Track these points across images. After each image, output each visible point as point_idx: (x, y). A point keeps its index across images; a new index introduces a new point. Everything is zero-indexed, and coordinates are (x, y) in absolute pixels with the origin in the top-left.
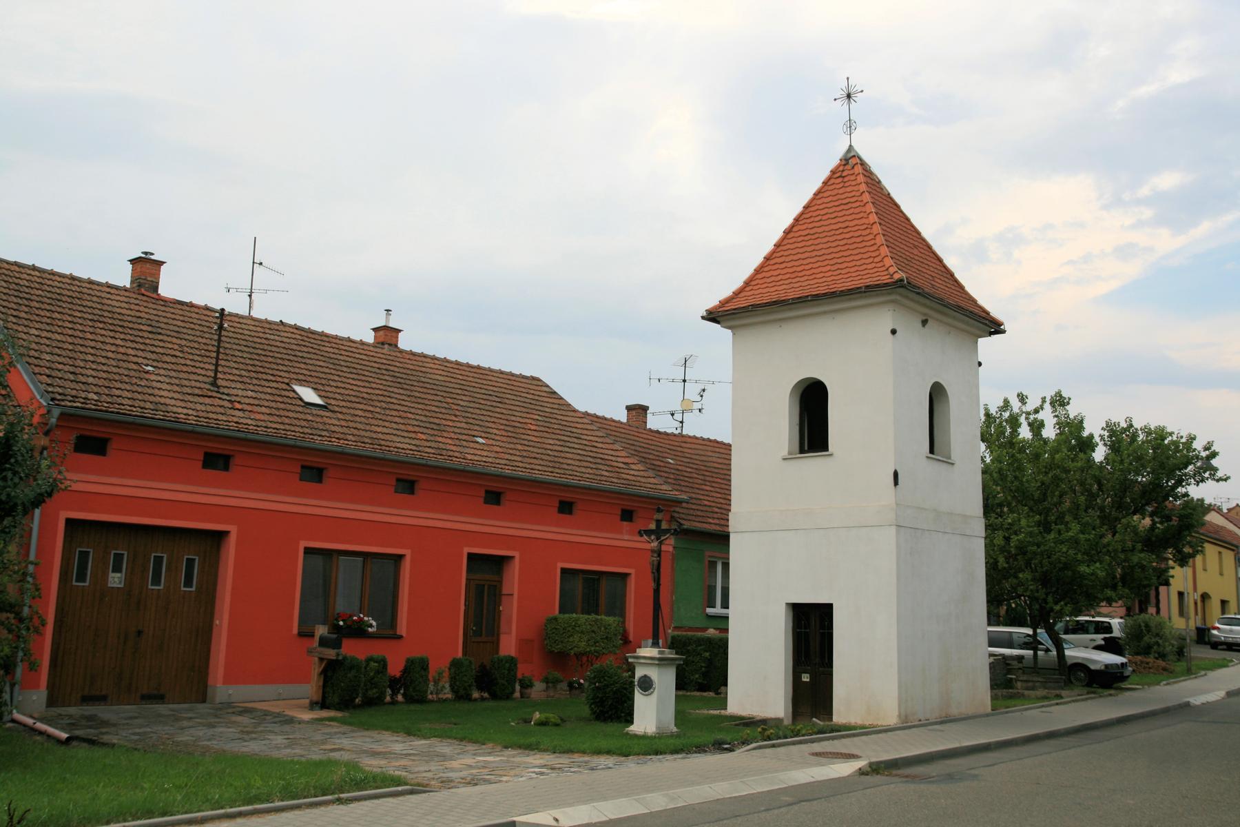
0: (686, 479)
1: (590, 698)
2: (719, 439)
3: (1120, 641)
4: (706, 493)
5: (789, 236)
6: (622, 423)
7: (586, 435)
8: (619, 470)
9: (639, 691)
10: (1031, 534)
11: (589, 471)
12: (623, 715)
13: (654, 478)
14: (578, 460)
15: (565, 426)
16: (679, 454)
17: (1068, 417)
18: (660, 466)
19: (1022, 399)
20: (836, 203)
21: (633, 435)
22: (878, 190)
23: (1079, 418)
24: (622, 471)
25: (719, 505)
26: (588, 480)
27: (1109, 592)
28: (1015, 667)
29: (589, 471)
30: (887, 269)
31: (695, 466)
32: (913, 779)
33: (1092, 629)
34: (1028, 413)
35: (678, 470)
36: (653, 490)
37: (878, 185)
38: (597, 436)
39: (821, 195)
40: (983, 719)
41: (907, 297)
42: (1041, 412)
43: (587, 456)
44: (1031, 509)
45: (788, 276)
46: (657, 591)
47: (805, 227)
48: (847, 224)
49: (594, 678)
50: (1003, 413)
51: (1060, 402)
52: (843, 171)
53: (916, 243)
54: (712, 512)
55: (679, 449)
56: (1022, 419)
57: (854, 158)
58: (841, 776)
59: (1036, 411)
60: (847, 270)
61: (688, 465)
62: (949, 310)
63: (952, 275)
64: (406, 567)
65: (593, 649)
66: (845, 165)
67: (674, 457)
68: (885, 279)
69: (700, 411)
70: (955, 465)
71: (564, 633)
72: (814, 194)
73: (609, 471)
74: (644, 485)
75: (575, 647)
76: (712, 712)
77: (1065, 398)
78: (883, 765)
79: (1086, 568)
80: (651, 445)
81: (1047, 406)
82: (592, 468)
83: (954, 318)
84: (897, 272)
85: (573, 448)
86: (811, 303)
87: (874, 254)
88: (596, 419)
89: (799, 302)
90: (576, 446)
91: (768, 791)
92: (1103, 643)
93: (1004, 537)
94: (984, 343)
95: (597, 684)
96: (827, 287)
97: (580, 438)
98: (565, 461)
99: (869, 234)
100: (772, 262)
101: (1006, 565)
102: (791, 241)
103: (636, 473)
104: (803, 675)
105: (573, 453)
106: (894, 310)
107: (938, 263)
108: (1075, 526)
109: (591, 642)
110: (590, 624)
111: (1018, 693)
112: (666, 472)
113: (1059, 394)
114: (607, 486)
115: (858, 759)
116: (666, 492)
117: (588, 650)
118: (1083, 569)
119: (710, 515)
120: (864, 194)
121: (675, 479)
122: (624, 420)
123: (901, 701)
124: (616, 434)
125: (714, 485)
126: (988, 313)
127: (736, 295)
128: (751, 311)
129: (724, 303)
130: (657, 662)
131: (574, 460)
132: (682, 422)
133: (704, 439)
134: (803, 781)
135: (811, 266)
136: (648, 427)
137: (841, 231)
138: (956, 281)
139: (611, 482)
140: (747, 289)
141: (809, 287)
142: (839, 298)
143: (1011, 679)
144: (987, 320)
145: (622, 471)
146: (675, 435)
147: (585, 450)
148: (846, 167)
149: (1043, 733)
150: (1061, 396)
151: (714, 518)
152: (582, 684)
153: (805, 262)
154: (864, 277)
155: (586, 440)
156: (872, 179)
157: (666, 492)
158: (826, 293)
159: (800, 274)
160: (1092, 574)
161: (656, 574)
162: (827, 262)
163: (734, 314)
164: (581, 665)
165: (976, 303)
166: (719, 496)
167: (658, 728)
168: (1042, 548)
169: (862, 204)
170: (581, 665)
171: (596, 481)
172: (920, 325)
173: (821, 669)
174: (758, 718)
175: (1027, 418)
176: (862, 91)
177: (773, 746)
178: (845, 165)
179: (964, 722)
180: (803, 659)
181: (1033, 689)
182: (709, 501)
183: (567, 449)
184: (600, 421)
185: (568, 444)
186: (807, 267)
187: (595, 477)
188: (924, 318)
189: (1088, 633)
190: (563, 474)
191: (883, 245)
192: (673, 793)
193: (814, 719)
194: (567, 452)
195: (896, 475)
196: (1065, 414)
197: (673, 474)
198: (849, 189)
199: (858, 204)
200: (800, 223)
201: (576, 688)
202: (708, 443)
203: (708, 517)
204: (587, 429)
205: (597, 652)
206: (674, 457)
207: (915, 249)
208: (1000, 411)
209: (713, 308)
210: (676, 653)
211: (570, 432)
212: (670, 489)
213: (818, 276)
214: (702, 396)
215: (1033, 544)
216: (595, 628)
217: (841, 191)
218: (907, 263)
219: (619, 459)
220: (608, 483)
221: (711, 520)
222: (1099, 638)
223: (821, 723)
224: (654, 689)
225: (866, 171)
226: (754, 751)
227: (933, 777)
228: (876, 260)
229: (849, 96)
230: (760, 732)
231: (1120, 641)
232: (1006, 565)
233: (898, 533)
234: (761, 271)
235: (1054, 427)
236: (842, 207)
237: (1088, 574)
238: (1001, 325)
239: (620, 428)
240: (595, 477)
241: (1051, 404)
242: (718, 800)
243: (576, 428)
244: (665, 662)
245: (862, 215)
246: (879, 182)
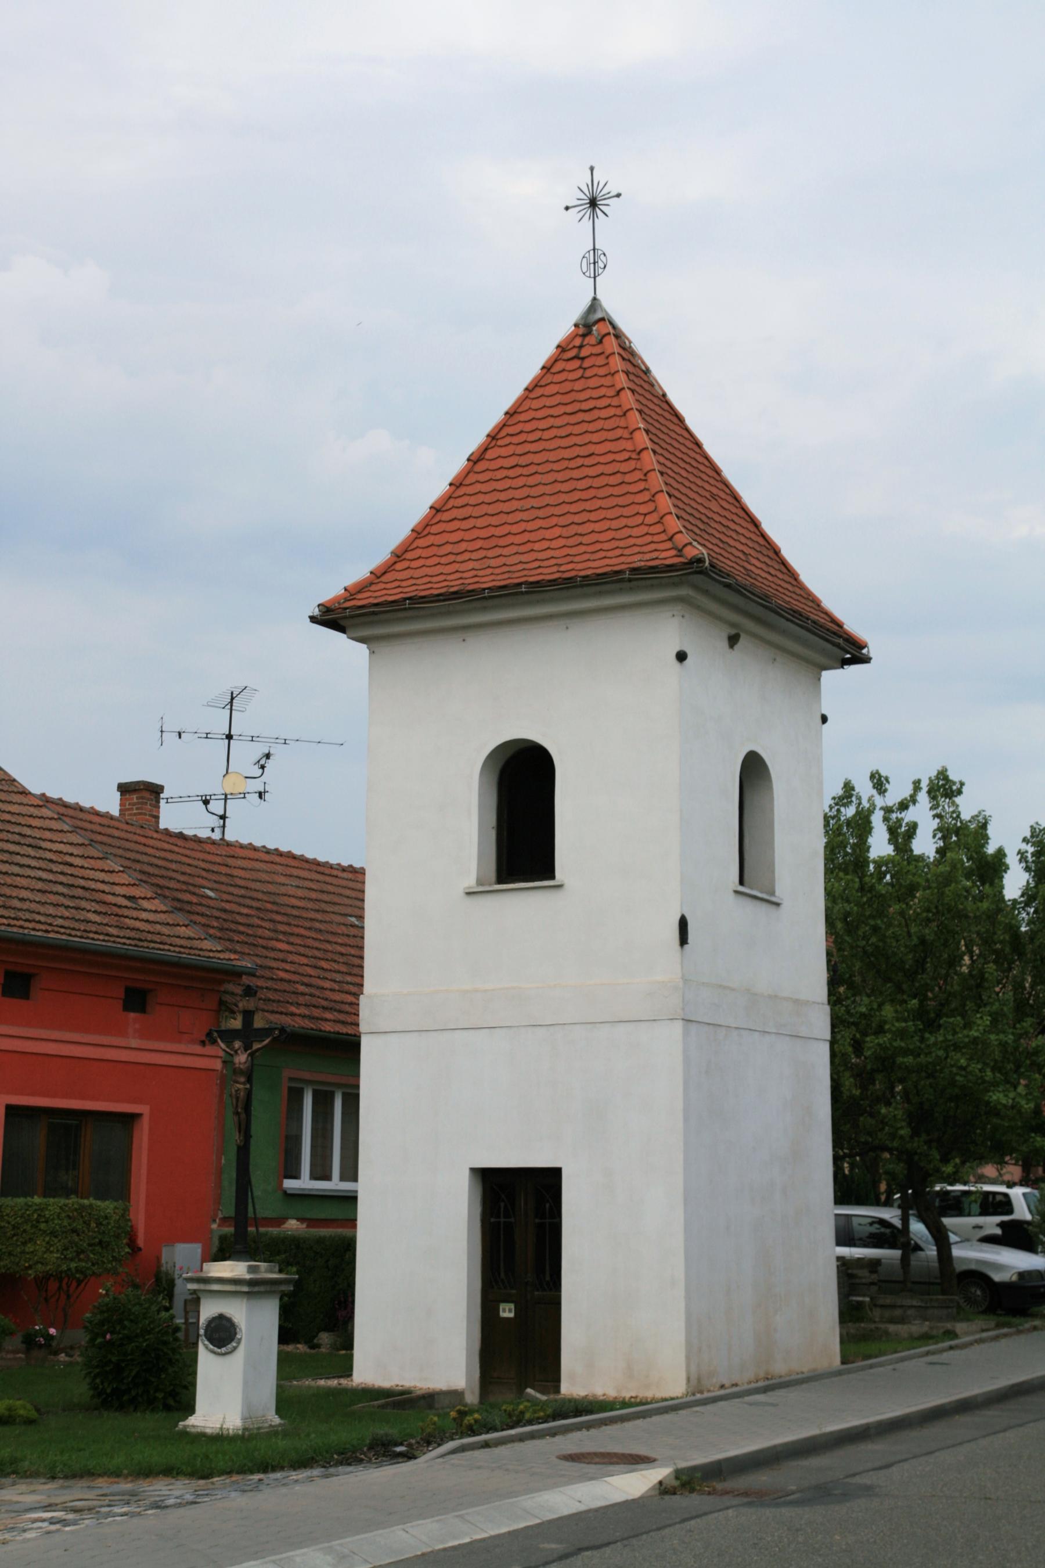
0: (241, 928)
1: (95, 1363)
2: (297, 852)
3: (1030, 1228)
4: (281, 955)
5: (481, 466)
6: (112, 818)
7: (51, 841)
8: (120, 912)
9: (207, 1348)
10: (902, 1034)
11: (62, 911)
12: (160, 1395)
13: (186, 926)
14: (38, 891)
15: (9, 822)
16: (223, 879)
17: (958, 816)
18: (189, 903)
19: (879, 782)
20: (569, 409)
21: (136, 842)
22: (646, 386)
23: (980, 818)
24: (126, 912)
25: (306, 980)
26: (62, 930)
27: (1039, 1139)
28: (864, 1281)
29: (62, 911)
30: (671, 539)
31: (254, 904)
32: (757, 1498)
33: (976, 1208)
34: (888, 810)
35: (225, 911)
36: (187, 951)
37: (645, 378)
38: (71, 844)
39: (538, 392)
40: (834, 1379)
41: (706, 592)
42: (911, 808)
43: (56, 882)
44: (899, 989)
45: (479, 544)
46: (243, 1152)
47: (510, 450)
48: (591, 449)
49: (102, 1323)
50: (842, 809)
51: (945, 789)
52: (581, 347)
53: (715, 491)
54: (294, 993)
55: (224, 870)
56: (877, 819)
57: (601, 323)
58: (630, 1498)
59: (903, 806)
60: (595, 537)
61: (242, 900)
62: (777, 617)
63: (777, 552)
64: (143, 1136)
65: (73, 1265)
66: (584, 336)
67: (215, 886)
68: (668, 557)
69: (260, 797)
70: (782, 906)
71: (14, 1235)
72: (527, 389)
73: (101, 913)
74: (168, 940)
75: (37, 1262)
76: (322, 1382)
77: (954, 783)
78: (698, 1475)
79: (1001, 1095)
80: (172, 861)
81: (923, 797)
82: (67, 907)
83: (784, 632)
84: (690, 544)
85: (29, 866)
86: (526, 597)
87: (643, 509)
88: (63, 810)
89: (501, 596)
90: (34, 863)
91: (509, 1532)
92: (998, 1231)
93: (854, 1039)
94: (832, 679)
95: (108, 1336)
96: (555, 569)
97: (40, 848)
98: (15, 893)
99: (635, 469)
100: (446, 516)
101: (857, 1092)
102: (482, 477)
103: (151, 917)
104: (502, 1306)
105: (29, 877)
106: (683, 616)
107: (753, 529)
108: (981, 1018)
109: (70, 1254)
110: (69, 1217)
111: (877, 1328)
112: (202, 915)
113: (943, 774)
114: (99, 942)
115: (651, 1465)
116: (211, 954)
117: (64, 1267)
118: (997, 1097)
119: (292, 998)
120: (622, 393)
121: (221, 929)
122: (115, 812)
123: (692, 1351)
124: (105, 839)
125: (292, 939)
126: (840, 625)
127: (378, 578)
128: (410, 609)
129: (351, 592)
130: (245, 1289)
131: (32, 890)
132: (223, 817)
133: (268, 852)
134: (566, 1511)
135: (523, 526)
136: (162, 826)
137: (579, 462)
138: (784, 563)
139: (107, 935)
140: (398, 566)
141: (520, 567)
142: (579, 591)
143: (860, 1304)
144: (841, 637)
145: (126, 912)
146: (213, 843)
147: (51, 871)
148: (587, 340)
149: (950, 1403)
150: (946, 778)
151: (298, 1005)
152: (52, 1337)
153: (510, 518)
154: (627, 552)
155: (50, 851)
156: (634, 366)
157: (211, 954)
158: (554, 580)
159: (502, 542)
160: (1013, 1107)
161: (243, 1116)
162: (554, 521)
163: (374, 613)
164: (46, 1300)
165: (819, 605)
166: (305, 961)
167: (244, 1419)
168: (922, 1059)
169: (619, 412)
170: (46, 1300)
171: (79, 934)
172: (725, 644)
173: (536, 1293)
174: (419, 1393)
175: (886, 819)
176: (618, 195)
177: (486, 1445)
178: (584, 336)
179: (804, 1386)
180: (503, 1275)
181: (902, 1320)
182: (287, 971)
183: (16, 869)
184: (71, 812)
185: (18, 859)
186: (515, 529)
187: (76, 925)
188: (733, 632)
189: (969, 1215)
190: (14, 919)
191: (662, 491)
192: (341, 1545)
193: (529, 1390)
194: (18, 875)
195: (683, 924)
196: (953, 812)
197: (217, 918)
198: (593, 382)
199: (611, 412)
200: (499, 443)
201: (41, 1346)
202: (278, 859)
203: (288, 1002)
204: (50, 830)
205: (82, 1272)
206: (215, 886)
207: (714, 502)
208: (836, 804)
209: (333, 600)
210: (280, 1271)
211: (20, 834)
212: (219, 949)
213: (536, 546)
214: (263, 767)
215: (906, 1052)
216: (79, 1225)
217: (578, 386)
218: (702, 527)
219: (118, 890)
220: (101, 937)
221: (293, 1009)
222: (991, 1223)
223: (544, 1398)
224: (239, 1342)
225: (624, 349)
226: (453, 1456)
227: (793, 1493)
228: (649, 520)
229: (593, 203)
230: (454, 1419)
231: (1030, 1228)
232: (857, 1092)
233: (686, 1034)
234: (425, 532)
235: (934, 836)
236: (581, 416)
237: (1005, 1106)
238: (863, 648)
239: (109, 826)
240: (76, 925)
241: (929, 792)
242: (423, 1554)
243: (30, 826)
244: (262, 1289)
245: (619, 433)
246: (647, 371)
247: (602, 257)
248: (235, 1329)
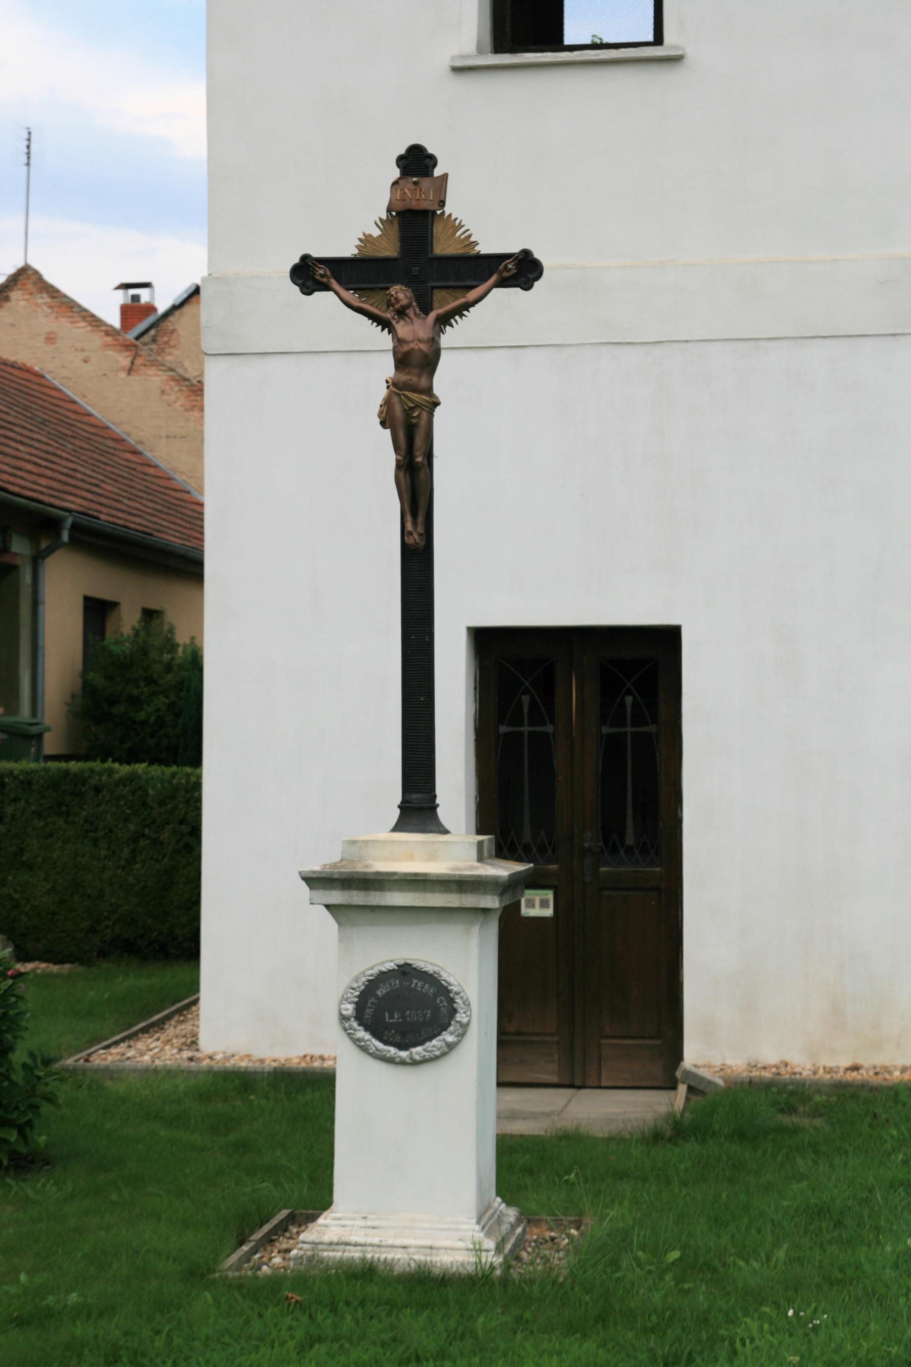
248: (452, 1001)
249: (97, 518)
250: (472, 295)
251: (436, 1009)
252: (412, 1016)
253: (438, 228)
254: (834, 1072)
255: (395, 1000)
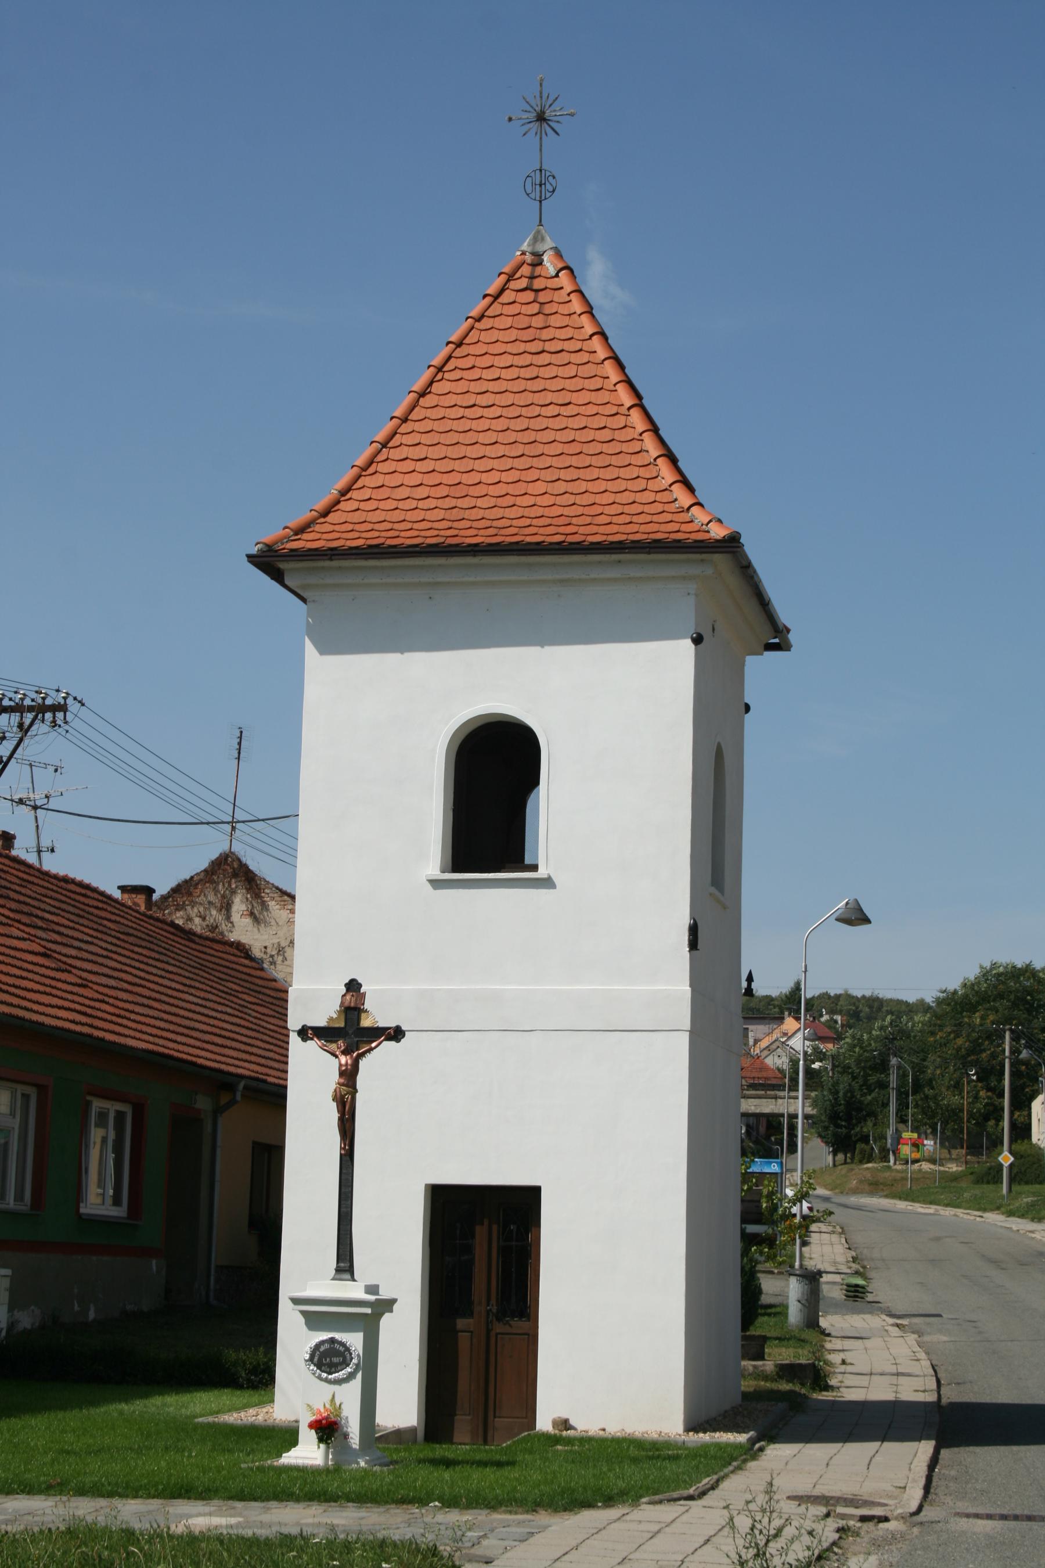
52: (532, 278)
200: (447, 376)
247: (551, 178)
249: (265, 1081)
250: (373, 1045)
251: (345, 1358)
252: (335, 1360)
253: (363, 1015)
254: (700, 1456)
255: (325, 1354)
